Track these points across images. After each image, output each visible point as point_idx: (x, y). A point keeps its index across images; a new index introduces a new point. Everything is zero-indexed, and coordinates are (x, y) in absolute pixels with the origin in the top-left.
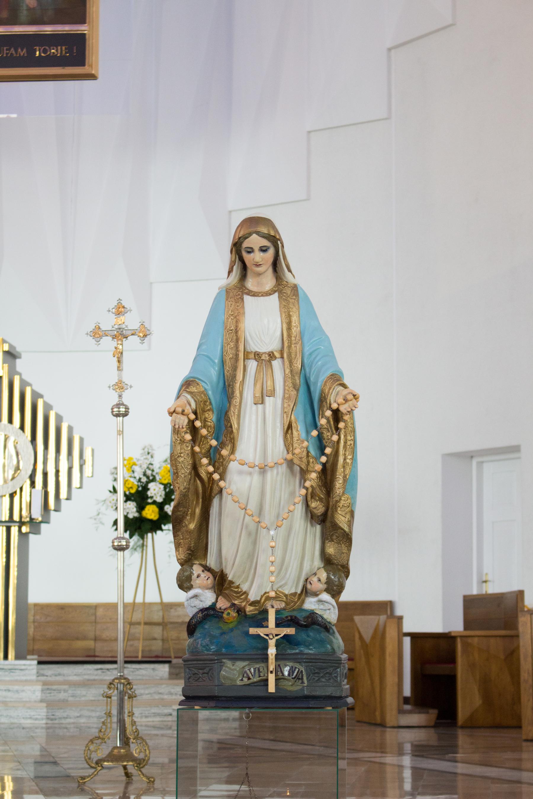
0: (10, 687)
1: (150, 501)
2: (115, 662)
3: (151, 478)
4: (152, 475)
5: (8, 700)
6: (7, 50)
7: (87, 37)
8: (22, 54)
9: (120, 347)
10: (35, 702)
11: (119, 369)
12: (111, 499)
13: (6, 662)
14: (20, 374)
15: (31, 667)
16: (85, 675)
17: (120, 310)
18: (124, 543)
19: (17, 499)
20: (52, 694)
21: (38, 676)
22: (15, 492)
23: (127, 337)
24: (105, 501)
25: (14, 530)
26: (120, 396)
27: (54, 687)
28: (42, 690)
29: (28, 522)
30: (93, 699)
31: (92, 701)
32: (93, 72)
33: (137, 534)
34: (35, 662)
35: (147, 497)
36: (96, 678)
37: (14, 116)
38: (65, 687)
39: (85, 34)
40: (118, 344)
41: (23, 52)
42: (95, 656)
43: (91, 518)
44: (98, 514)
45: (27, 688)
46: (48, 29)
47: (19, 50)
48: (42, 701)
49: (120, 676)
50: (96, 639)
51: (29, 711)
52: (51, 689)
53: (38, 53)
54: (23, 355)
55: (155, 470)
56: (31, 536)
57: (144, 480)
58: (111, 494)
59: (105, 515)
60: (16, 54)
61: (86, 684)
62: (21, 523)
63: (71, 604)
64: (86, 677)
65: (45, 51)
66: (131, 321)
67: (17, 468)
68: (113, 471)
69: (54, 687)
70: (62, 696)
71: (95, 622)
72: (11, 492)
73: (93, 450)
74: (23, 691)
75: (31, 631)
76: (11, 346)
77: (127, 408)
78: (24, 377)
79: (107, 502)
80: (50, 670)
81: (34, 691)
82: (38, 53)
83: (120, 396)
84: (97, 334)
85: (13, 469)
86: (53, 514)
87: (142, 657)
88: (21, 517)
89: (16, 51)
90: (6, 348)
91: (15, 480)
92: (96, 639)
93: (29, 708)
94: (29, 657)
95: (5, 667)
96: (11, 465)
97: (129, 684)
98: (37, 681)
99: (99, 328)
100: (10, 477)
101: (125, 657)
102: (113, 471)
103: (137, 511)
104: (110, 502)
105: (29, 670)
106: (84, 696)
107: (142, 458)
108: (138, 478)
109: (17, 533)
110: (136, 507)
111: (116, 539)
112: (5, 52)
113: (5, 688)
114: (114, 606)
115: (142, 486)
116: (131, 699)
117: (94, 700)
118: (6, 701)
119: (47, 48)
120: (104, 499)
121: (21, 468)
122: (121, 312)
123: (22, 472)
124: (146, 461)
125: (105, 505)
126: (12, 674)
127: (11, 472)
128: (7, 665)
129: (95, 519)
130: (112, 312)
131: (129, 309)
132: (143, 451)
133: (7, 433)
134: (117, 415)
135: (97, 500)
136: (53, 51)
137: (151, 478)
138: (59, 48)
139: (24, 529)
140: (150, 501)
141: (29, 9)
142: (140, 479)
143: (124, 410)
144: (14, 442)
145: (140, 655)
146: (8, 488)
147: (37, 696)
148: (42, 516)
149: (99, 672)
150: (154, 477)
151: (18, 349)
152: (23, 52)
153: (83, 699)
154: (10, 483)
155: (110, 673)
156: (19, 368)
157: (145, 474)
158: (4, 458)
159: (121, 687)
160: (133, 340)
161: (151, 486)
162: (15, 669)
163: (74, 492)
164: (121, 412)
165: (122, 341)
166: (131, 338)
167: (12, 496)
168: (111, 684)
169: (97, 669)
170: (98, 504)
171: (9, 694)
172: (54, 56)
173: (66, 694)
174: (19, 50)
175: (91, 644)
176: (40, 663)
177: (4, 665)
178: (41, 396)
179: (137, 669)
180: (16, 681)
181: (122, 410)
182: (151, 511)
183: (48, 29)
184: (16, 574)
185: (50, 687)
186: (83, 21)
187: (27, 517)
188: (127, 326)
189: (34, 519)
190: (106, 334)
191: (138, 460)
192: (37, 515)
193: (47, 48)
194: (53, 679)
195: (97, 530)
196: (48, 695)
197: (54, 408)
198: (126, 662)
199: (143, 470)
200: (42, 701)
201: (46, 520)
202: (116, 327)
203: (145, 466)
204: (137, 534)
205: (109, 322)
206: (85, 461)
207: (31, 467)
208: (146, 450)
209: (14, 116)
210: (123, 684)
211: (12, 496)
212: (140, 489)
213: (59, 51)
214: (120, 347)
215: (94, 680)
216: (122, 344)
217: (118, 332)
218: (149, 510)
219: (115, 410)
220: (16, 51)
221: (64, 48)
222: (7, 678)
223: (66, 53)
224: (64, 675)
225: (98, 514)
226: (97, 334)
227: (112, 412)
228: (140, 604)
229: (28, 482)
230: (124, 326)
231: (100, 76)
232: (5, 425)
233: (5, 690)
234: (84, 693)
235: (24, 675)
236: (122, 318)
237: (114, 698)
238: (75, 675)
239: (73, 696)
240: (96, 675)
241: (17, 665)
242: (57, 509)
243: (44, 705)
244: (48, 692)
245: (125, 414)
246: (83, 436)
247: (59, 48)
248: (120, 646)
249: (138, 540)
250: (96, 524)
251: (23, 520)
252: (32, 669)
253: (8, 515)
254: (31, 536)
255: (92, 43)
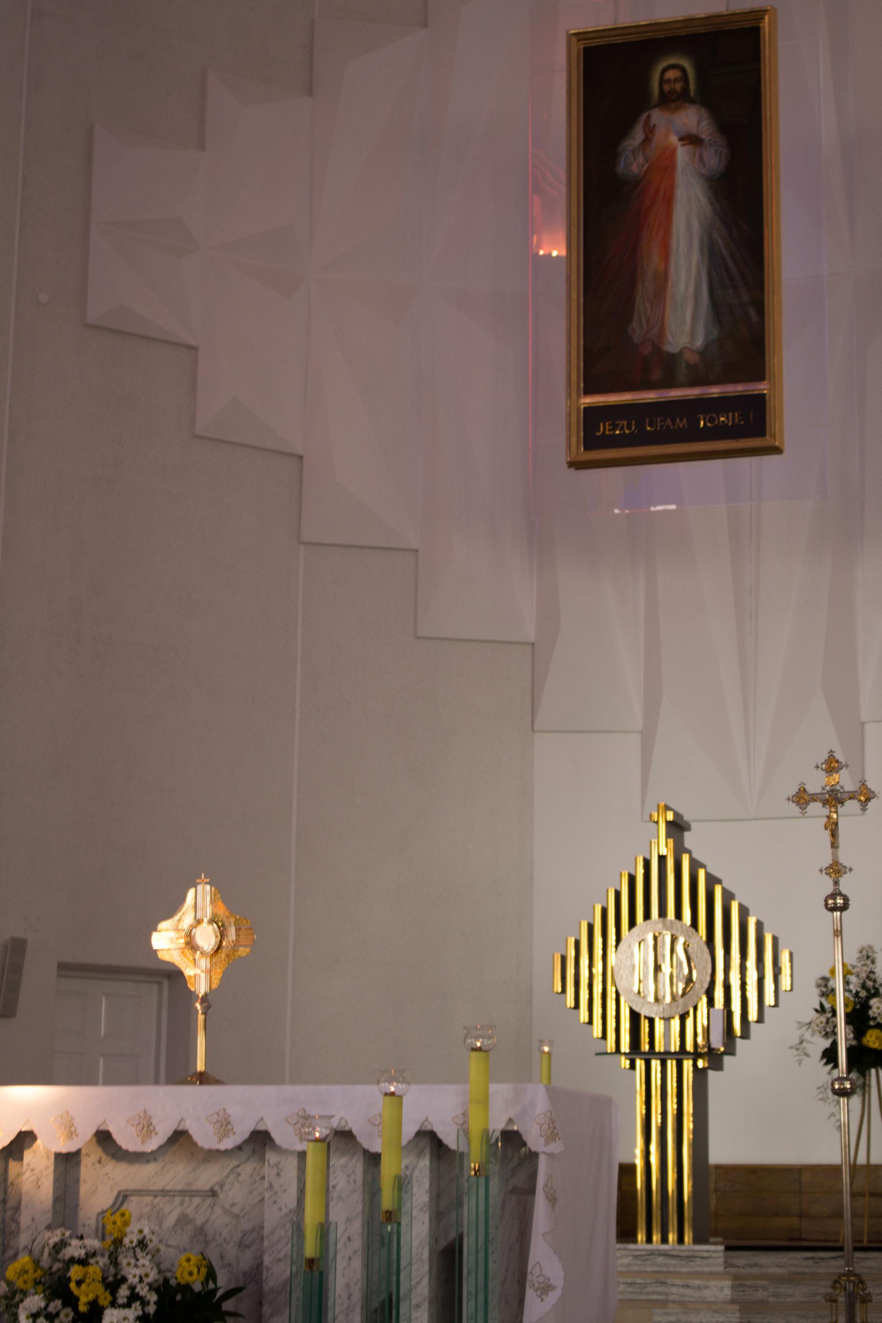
0: (690, 1282)
1: (872, 1023)
2: (841, 1249)
3: (872, 991)
4: (874, 987)
5: (686, 1299)
6: (661, 421)
7: (767, 397)
8: (681, 426)
9: (835, 816)
10: (724, 1302)
11: (834, 845)
12: (818, 1022)
13: (683, 1247)
14: (689, 852)
15: (716, 1255)
16: (790, 1265)
17: (832, 765)
18: (848, 1086)
19: (689, 1022)
20: (747, 1293)
21: (726, 1267)
22: (688, 1013)
23: (842, 803)
24: (810, 1023)
25: (688, 1065)
26: (836, 883)
27: (749, 1283)
28: (733, 1287)
29: (705, 1053)
30: (803, 1300)
31: (801, 1302)
32: (777, 444)
33: (855, 1070)
34: (721, 1248)
35: (869, 1018)
36: (806, 1270)
37: (673, 507)
38: (765, 1283)
39: (764, 395)
40: (831, 812)
41: (682, 423)
42: (801, 1239)
43: (791, 1048)
44: (801, 1042)
45: (712, 1283)
46: (715, 391)
47: (678, 421)
48: (732, 1302)
49: (849, 1271)
50: (801, 1215)
51: (716, 1315)
52: (745, 1286)
53: (702, 423)
54: (693, 826)
55: (878, 980)
56: (711, 1074)
57: (863, 994)
58: (817, 1015)
59: (811, 1043)
60: (674, 425)
61: (792, 1279)
62: (696, 1055)
63: (774, 1165)
64: (792, 1269)
65: (711, 420)
66: (845, 780)
67: (689, 980)
68: (820, 982)
69: (749, 1283)
70: (760, 1295)
71: (800, 1192)
72: (681, 1013)
73: (791, 954)
74: (707, 1287)
75: (713, 1203)
76: (676, 814)
77: (846, 899)
78: (695, 855)
79: (814, 1026)
80: (743, 1259)
81: (722, 1287)
82: (702, 423)
83: (836, 883)
84: (802, 798)
85: (684, 981)
86: (739, 1043)
87: (869, 1241)
88: (696, 1044)
89: (674, 423)
90: (670, 816)
91: (686, 997)
92: (801, 1215)
93: (716, 1311)
94: (712, 1240)
95: (682, 1254)
96: (681, 976)
97: (861, 1282)
98: (725, 1273)
99: (805, 790)
100: (680, 992)
101: (854, 1241)
102: (820, 982)
103: (855, 1038)
104: (817, 1026)
105: (714, 1258)
106: (791, 1296)
107: (859, 965)
108: (854, 991)
109: (691, 1069)
110: (853, 1032)
111: (836, 1080)
112: (659, 424)
113: (683, 1283)
114: (833, 1171)
115: (860, 1002)
116: (210, 1194)
117: (805, 1302)
118: (683, 1302)
119: (715, 416)
120: (808, 1021)
121: (694, 979)
122: (834, 768)
123: (696, 985)
124: (865, 968)
125: (810, 1030)
126: (691, 1263)
127: (681, 986)
128: (684, 1251)
129: (797, 1049)
130: (822, 769)
131: (844, 763)
132: (859, 955)
133: (675, 932)
134: (833, 909)
135: (799, 1023)
136: (722, 419)
137: (872, 991)
138: (731, 414)
139: (701, 1064)
140: (872, 1023)
141: (689, 366)
142: (857, 993)
143: (842, 901)
144: (684, 944)
145: (865, 1238)
146: (678, 1007)
147: (726, 1295)
148: (725, 1045)
149: (810, 1262)
150: (877, 990)
151: (686, 818)
152: (682, 423)
153: (789, 1300)
154: (681, 1001)
155: (833, 1264)
156: (687, 844)
157: (864, 986)
158: (672, 967)
159: (850, 1287)
160: (852, 806)
161: (874, 1002)
162: (697, 1257)
163: (767, 1012)
164: (837, 903)
165: (837, 808)
166: (848, 803)
167: (683, 1018)
168: (836, 1282)
169: (807, 1259)
170: (800, 1028)
171: (687, 1291)
172: (724, 425)
173: (766, 1293)
174: (678, 421)
175: (794, 1222)
176: (728, 1248)
177: (679, 1250)
178: (719, 882)
179: (864, 1259)
180: (697, 1273)
181: (840, 901)
182: (874, 1038)
183: (715, 391)
184: (691, 1126)
185: (743, 1282)
186: (760, 376)
187: (704, 1047)
188: (842, 787)
189: (714, 1049)
190: (814, 798)
191: (854, 967)
192: (717, 1042)
193: (715, 416)
194: (748, 1271)
195: (800, 1064)
196: (742, 1294)
197: (737, 897)
198: (856, 1249)
199: (862, 981)
200: (732, 1302)
201: (730, 1050)
202: (828, 788)
203: (864, 975)
204: (855, 1070)
205: (817, 783)
206: (780, 969)
207: (708, 979)
208: (864, 952)
209: (673, 507)
210: (854, 1283)
211: (683, 1018)
212: (858, 1007)
213: (731, 418)
214: (835, 816)
215: (803, 1273)
216: (836, 812)
217: (830, 795)
218: (871, 1036)
219: (830, 902)
220: (674, 423)
221: (736, 415)
222: (685, 1270)
223: (740, 421)
224: (761, 1266)
225: (801, 1042)
226: (802, 798)
227: (826, 905)
228: (862, 1166)
229: (705, 999)
230: (838, 788)
231: (786, 448)
232: (671, 921)
233: (683, 1286)
234: (790, 1291)
235: (708, 1265)
236: (836, 776)
237: (841, 1299)
238: (778, 1266)
239: (774, 1296)
240: (806, 1267)
241: (697, 1251)
242: (745, 1035)
243: (737, 1307)
244: (741, 1289)
245: (844, 908)
246: (777, 935)
247: (731, 414)
248: (847, 1231)
249: (858, 1078)
250: (799, 1055)
251: (699, 1050)
252: (719, 1257)
253: (678, 1044)
254: (711, 1074)
255: (775, 406)
